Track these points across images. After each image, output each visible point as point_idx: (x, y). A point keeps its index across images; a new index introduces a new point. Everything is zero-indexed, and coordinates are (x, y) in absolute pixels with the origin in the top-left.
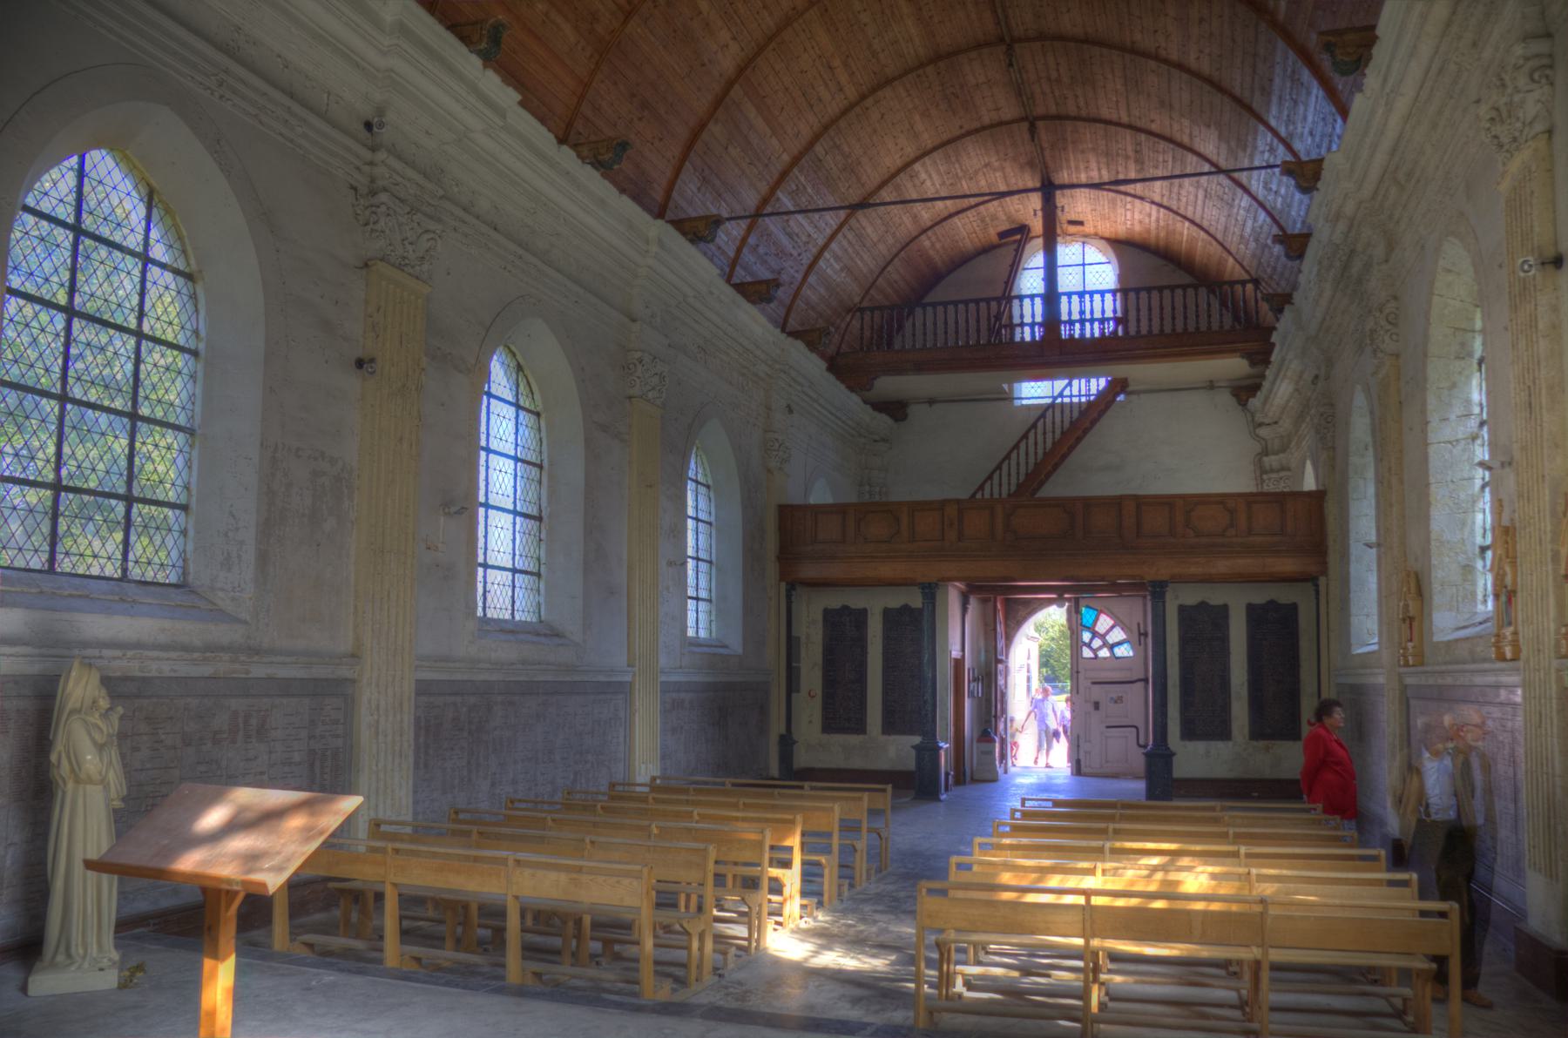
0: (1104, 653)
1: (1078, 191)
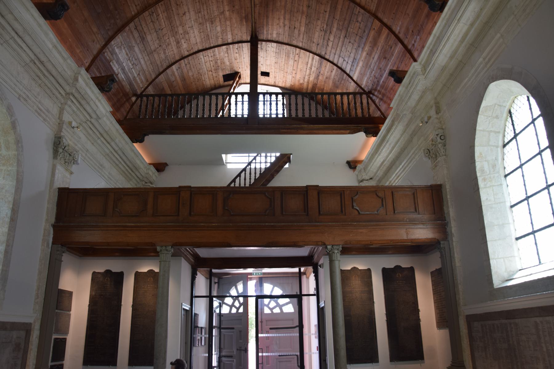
0: (277, 310)
1: (270, 44)
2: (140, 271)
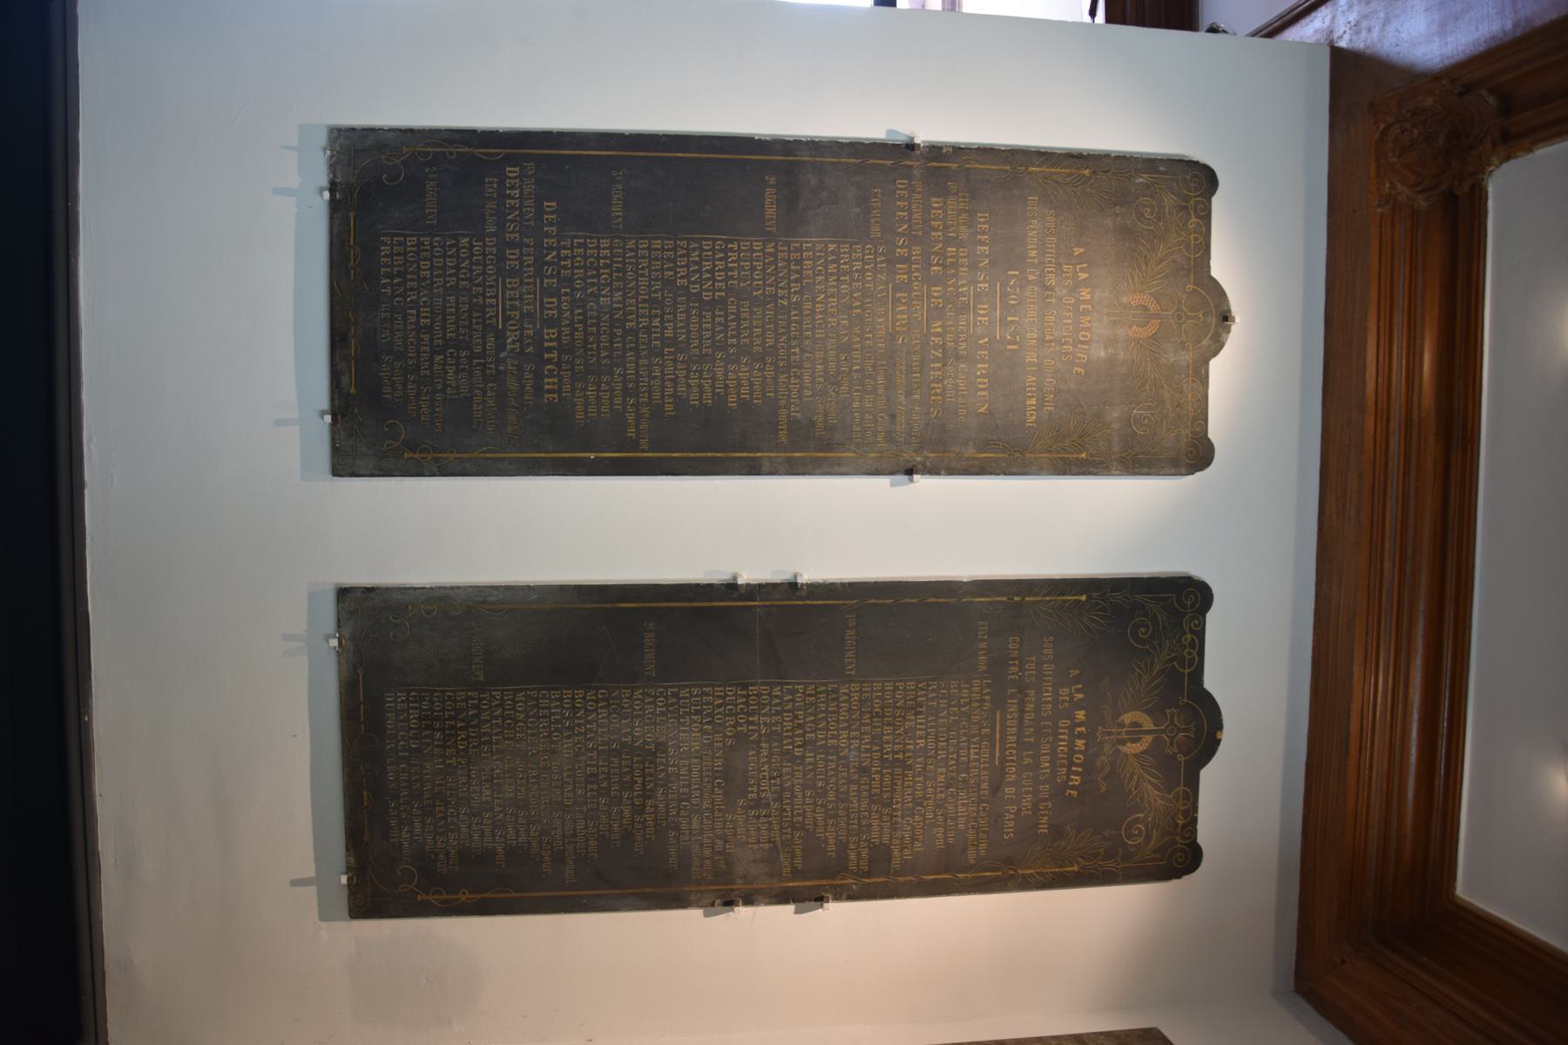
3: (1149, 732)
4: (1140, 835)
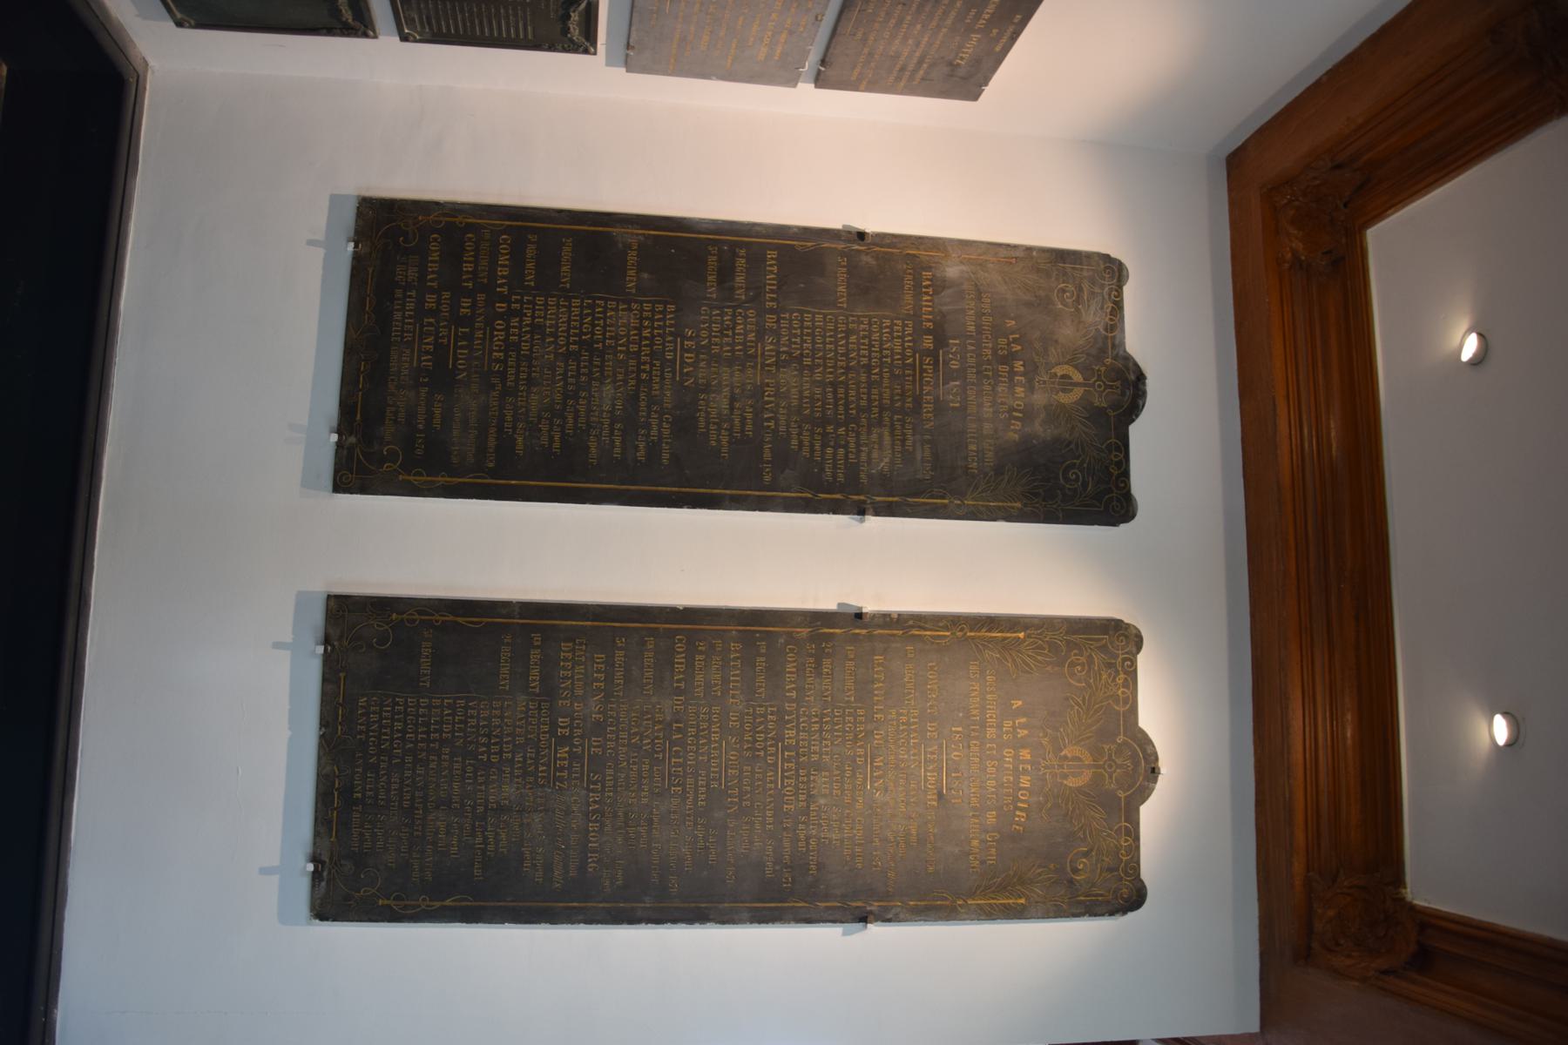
2: (1147, 665)
3: (1077, 384)
4: (1077, 479)
